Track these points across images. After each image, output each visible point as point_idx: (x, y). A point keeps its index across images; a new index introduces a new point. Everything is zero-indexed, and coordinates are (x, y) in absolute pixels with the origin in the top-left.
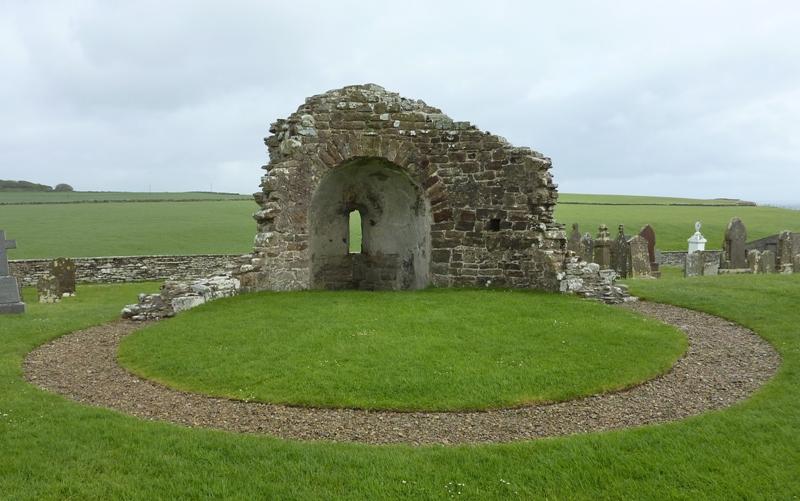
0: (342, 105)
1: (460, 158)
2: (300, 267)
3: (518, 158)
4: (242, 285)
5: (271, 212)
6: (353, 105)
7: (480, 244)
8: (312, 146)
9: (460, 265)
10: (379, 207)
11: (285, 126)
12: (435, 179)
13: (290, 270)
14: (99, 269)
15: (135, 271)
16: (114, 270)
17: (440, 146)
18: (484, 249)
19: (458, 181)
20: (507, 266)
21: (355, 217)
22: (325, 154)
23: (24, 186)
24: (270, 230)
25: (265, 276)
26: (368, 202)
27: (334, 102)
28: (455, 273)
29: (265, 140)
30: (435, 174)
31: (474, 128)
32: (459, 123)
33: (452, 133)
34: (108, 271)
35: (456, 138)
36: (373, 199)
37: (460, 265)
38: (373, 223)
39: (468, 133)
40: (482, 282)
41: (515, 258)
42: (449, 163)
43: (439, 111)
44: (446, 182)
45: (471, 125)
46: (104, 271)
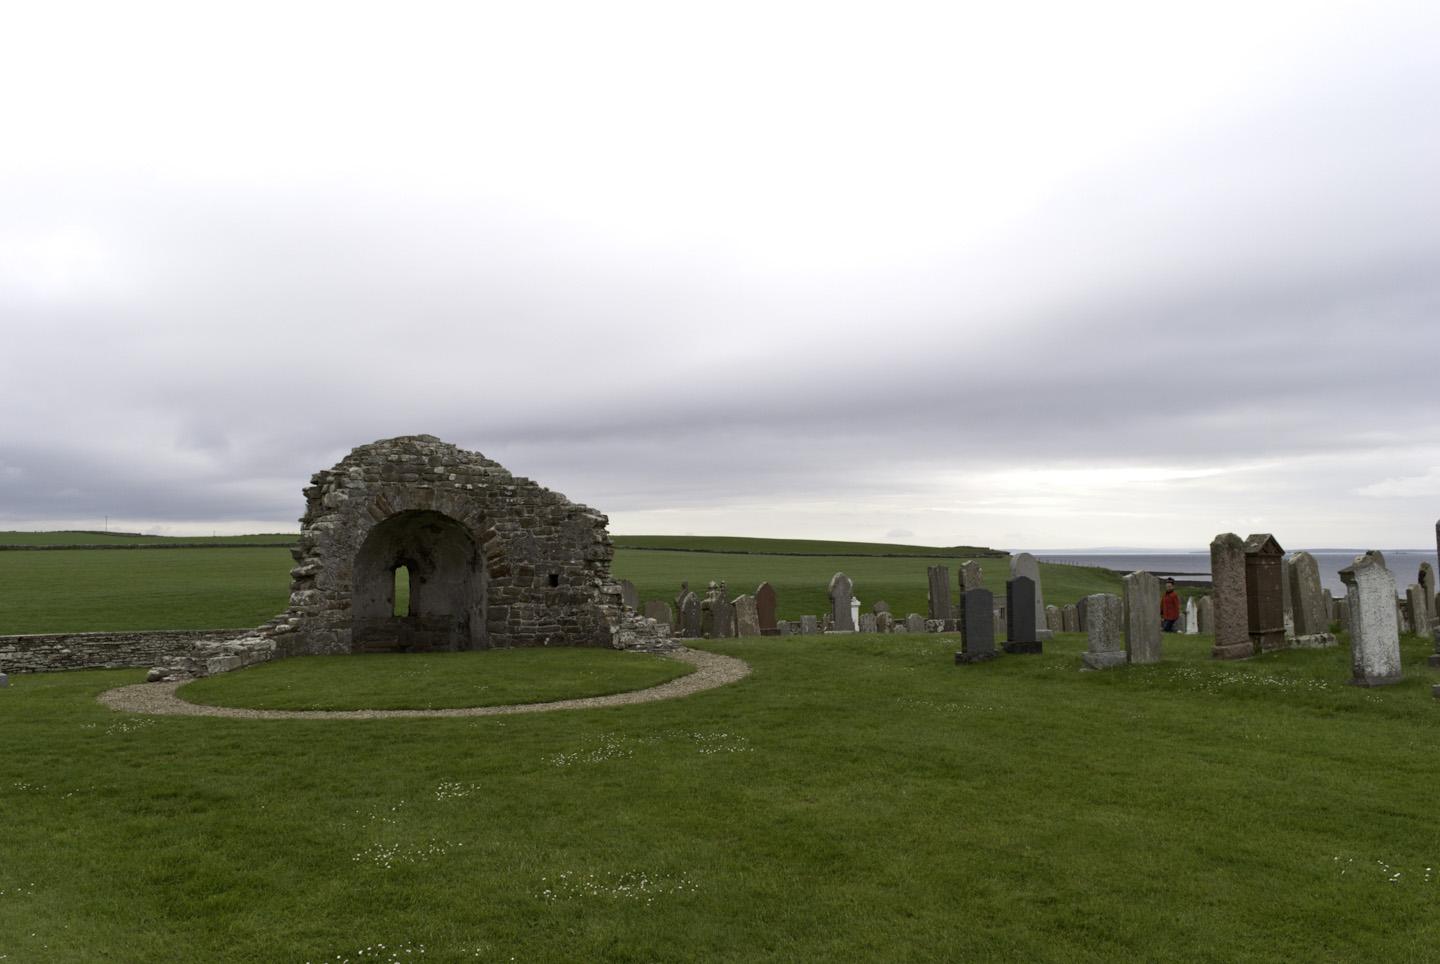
0: (394, 457)
1: (519, 513)
2: (342, 628)
4: (278, 646)
5: (313, 568)
6: (405, 457)
7: (538, 600)
9: (518, 623)
10: (431, 562)
11: (330, 478)
12: (493, 534)
16: (19, 655)
17: (497, 501)
18: (543, 606)
19: (517, 535)
20: (565, 622)
21: (402, 573)
22: (374, 507)
24: (310, 588)
26: (417, 557)
27: (384, 454)
28: (512, 631)
29: (304, 490)
30: (493, 529)
33: (510, 488)
34: (9, 656)
35: (514, 494)
36: (425, 554)
38: (423, 581)
40: (540, 641)
41: (573, 614)
42: (507, 518)
44: (504, 536)
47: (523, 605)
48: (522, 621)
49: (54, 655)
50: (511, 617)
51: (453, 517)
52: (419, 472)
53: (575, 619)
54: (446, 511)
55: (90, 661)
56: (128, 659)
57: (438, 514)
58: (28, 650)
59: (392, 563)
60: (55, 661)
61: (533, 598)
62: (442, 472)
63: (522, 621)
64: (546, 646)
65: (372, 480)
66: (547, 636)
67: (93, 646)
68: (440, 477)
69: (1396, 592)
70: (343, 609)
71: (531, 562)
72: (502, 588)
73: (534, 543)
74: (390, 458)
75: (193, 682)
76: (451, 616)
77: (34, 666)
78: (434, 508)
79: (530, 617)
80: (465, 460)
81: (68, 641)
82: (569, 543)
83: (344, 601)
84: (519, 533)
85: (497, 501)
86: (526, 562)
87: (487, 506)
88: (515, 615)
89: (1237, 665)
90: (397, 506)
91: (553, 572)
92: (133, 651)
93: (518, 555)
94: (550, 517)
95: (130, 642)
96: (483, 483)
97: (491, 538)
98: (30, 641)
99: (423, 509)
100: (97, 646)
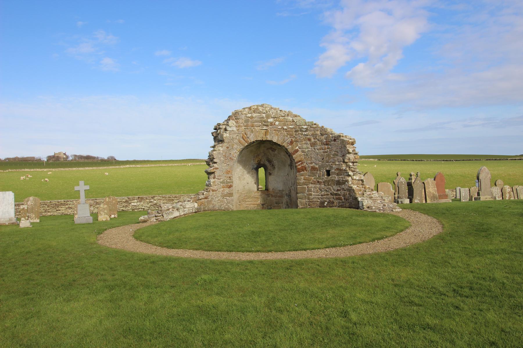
0: (249, 115)
2: (229, 197)
3: (337, 139)
4: (198, 205)
5: (213, 169)
6: (254, 115)
8: (235, 136)
9: (311, 195)
10: (273, 165)
13: (223, 198)
14: (130, 203)
15: (150, 204)
16: (138, 203)
17: (299, 134)
19: (309, 151)
21: (262, 170)
22: (242, 139)
23: (195, 159)
25: (211, 201)
26: (267, 163)
27: (245, 114)
30: (297, 148)
31: (315, 124)
32: (308, 122)
34: (135, 204)
35: (307, 130)
36: (270, 161)
37: (311, 195)
38: (270, 174)
39: (313, 127)
42: (304, 142)
43: (299, 116)
45: (314, 123)
46: (133, 204)
47: (313, 186)
48: (313, 193)
49: (151, 204)
50: (308, 191)
51: (279, 143)
52: (261, 122)
53: (339, 193)
54: (275, 140)
57: (271, 142)
58: (142, 202)
59: (255, 166)
60: (151, 205)
61: (318, 182)
62: (272, 121)
63: (313, 193)
64: (326, 207)
65: (239, 126)
66: (326, 201)
68: (271, 124)
69: (367, 172)
70: (229, 188)
71: (316, 164)
72: (303, 177)
73: (317, 155)
74: (247, 116)
75: (492, 201)
76: (283, 190)
77: (144, 207)
78: (269, 139)
79: (317, 192)
80: (283, 115)
81: (155, 198)
82: (335, 154)
83: (229, 184)
84: (310, 150)
85: (299, 134)
86: (314, 164)
87: (294, 137)
88: (309, 190)
90: (252, 138)
91: (328, 169)
93: (310, 160)
94: (325, 141)
95: (177, 198)
96: (292, 125)
98: (142, 198)
99: (264, 140)
100: (166, 200)
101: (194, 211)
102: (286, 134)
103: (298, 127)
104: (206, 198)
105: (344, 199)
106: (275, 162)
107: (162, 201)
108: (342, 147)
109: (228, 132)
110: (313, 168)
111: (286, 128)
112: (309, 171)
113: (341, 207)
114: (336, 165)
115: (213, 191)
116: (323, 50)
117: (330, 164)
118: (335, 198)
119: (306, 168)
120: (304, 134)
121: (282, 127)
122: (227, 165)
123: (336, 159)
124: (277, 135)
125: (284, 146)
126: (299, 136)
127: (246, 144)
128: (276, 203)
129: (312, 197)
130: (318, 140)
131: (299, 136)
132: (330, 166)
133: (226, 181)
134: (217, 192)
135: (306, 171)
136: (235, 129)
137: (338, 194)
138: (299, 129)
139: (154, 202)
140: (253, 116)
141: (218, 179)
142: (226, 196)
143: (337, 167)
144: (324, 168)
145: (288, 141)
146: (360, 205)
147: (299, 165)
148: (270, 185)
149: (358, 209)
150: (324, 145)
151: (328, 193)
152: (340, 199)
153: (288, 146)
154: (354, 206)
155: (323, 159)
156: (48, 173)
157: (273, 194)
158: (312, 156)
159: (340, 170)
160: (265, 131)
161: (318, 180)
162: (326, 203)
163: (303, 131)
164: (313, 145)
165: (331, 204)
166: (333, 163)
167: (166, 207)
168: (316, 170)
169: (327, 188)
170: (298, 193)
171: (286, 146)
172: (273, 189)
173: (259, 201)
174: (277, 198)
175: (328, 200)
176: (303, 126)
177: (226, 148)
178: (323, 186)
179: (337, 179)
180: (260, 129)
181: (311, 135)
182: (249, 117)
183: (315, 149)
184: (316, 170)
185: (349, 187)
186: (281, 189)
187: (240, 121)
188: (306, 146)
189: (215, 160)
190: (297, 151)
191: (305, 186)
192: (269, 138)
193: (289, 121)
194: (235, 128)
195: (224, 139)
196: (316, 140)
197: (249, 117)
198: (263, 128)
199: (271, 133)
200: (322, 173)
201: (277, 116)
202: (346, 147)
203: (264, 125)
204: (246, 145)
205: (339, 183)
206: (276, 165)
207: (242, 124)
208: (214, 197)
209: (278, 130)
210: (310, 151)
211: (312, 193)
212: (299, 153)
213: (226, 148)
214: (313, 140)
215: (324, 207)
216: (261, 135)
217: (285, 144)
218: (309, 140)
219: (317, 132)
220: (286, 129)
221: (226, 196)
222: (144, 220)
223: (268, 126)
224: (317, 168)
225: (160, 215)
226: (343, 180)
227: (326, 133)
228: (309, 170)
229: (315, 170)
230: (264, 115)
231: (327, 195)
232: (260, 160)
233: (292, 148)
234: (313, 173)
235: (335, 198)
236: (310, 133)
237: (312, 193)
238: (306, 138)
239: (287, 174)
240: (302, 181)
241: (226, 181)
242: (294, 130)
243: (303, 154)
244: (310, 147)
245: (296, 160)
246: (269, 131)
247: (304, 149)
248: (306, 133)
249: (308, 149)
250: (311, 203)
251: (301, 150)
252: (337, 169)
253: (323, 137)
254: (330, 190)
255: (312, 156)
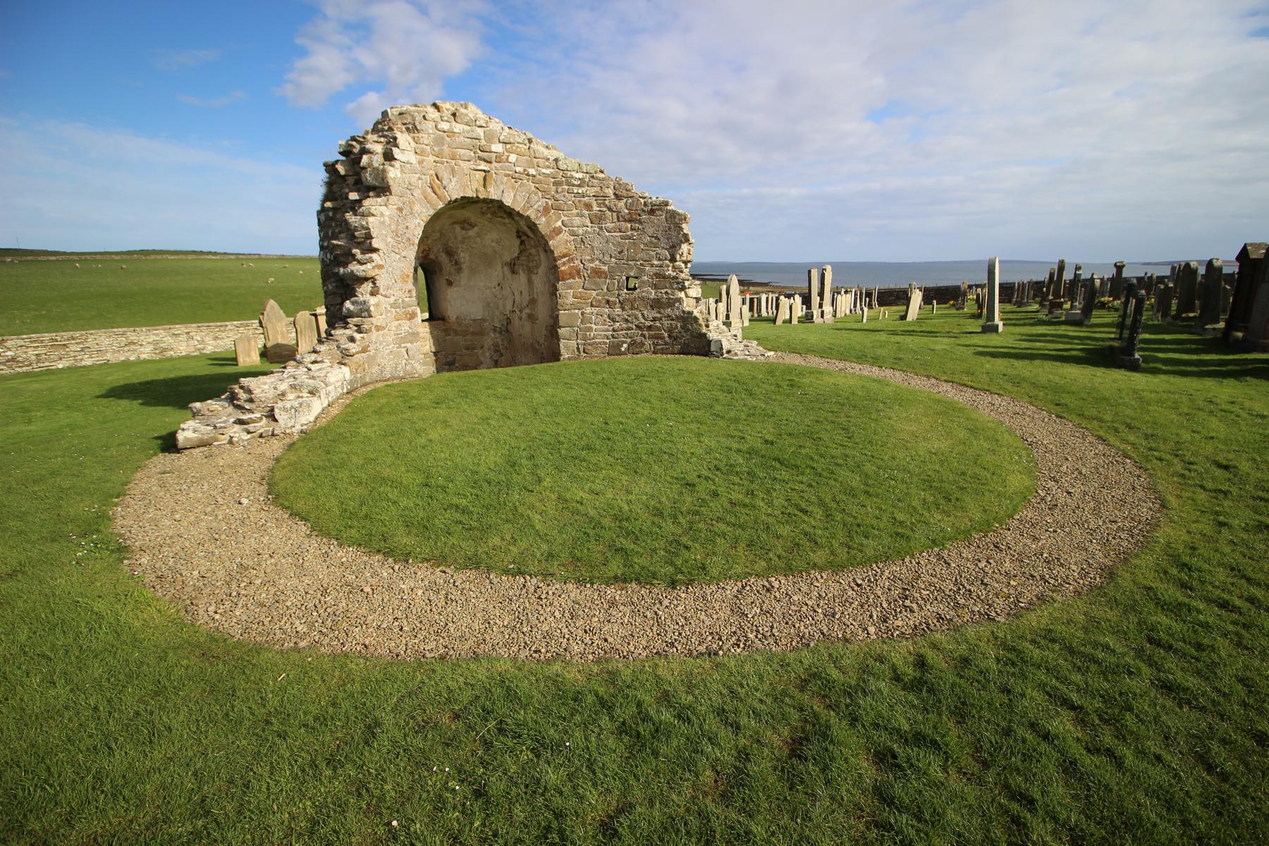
5: (374, 267)
9: (590, 329)
10: (457, 263)
22: (429, 190)
39: (597, 179)
48: (594, 327)
54: (508, 201)
55: (38, 361)
56: (79, 357)
61: (608, 302)
63: (594, 327)
64: (624, 353)
66: (625, 342)
67: (38, 347)
70: (410, 319)
76: (483, 320)
84: (589, 229)
86: (597, 262)
89: (892, 340)
90: (455, 191)
92: (82, 350)
95: (78, 341)
96: (548, 167)
97: (558, 234)
100: (45, 346)
101: (345, 391)
102: (533, 189)
103: (561, 173)
104: (364, 350)
105: (670, 336)
106: (463, 256)
107: (30, 349)
108: (670, 229)
109: (397, 164)
110: (597, 273)
111: (534, 173)
112: (587, 279)
113: (662, 354)
114: (652, 266)
115: (378, 328)
116: (303, 53)
117: (639, 263)
118: (647, 336)
119: (578, 272)
120: (575, 191)
121: (525, 170)
122: (402, 259)
123: (653, 253)
124: (513, 188)
125: (528, 217)
126: (564, 196)
127: (441, 205)
128: (467, 349)
129: (592, 334)
130: (610, 209)
131: (564, 196)
132: (639, 269)
133: (403, 301)
134: (386, 331)
135: (580, 278)
136: (413, 159)
137: (657, 326)
138: (564, 179)
139: (6, 354)
140: (455, 130)
141: (386, 296)
142: (404, 340)
143: (654, 270)
144: (622, 273)
145: (539, 206)
146: (713, 348)
147: (564, 264)
148: (449, 308)
149: (706, 354)
150: (625, 221)
151: (630, 325)
152: (661, 337)
153: (538, 218)
154: (694, 351)
155: (620, 253)
156: (1207, 327)
157: (459, 329)
158: (593, 245)
159: (664, 278)
160: (483, 174)
161: (607, 297)
162: (625, 345)
163: (574, 185)
164: (597, 219)
165: (635, 348)
166: (645, 261)
167: (267, 387)
168: (604, 276)
169: (629, 316)
170: (560, 327)
171: (533, 217)
172: (457, 318)
173: (428, 346)
174: (468, 337)
175: (629, 340)
176: (573, 173)
177: (397, 209)
178: (618, 310)
179: (653, 296)
180: (472, 167)
181: (594, 196)
182: (445, 132)
183: (601, 229)
184: (604, 276)
185: (684, 312)
186: (480, 318)
187: (425, 138)
188: (581, 223)
189: (375, 244)
190: (558, 231)
191: (576, 311)
192: (494, 194)
193: (541, 156)
194: (414, 157)
195: (391, 182)
196: (605, 209)
197: (445, 132)
198: (480, 168)
199: (498, 183)
200: (619, 282)
201: (512, 141)
202: (682, 229)
203: (480, 158)
204: (439, 207)
205: (656, 304)
206: (464, 263)
207: (429, 147)
208: (380, 345)
209: (515, 177)
210: (589, 233)
211: (593, 325)
212: (564, 236)
213: (397, 209)
214: (596, 208)
215: (621, 354)
216: (475, 185)
217: (531, 213)
218: (588, 206)
219: (606, 191)
220: (534, 176)
221: (404, 340)
222: (201, 440)
223: (490, 162)
224: (604, 272)
225: (259, 415)
226: (669, 299)
227: (630, 194)
228: (586, 275)
229: (600, 277)
230: (480, 132)
231: (629, 329)
232: (430, 249)
233: (548, 223)
234: (596, 284)
235: (647, 336)
236: (592, 191)
237: (593, 325)
238: (580, 201)
239: (496, 283)
240: (571, 300)
241: (403, 301)
242: (552, 180)
243: (572, 238)
244: (590, 225)
245: (555, 252)
246: (494, 175)
247: (575, 229)
248: (580, 191)
249: (584, 228)
250: (589, 347)
251: (567, 229)
252: (657, 275)
253: (621, 204)
254: (636, 318)
255: (596, 244)
